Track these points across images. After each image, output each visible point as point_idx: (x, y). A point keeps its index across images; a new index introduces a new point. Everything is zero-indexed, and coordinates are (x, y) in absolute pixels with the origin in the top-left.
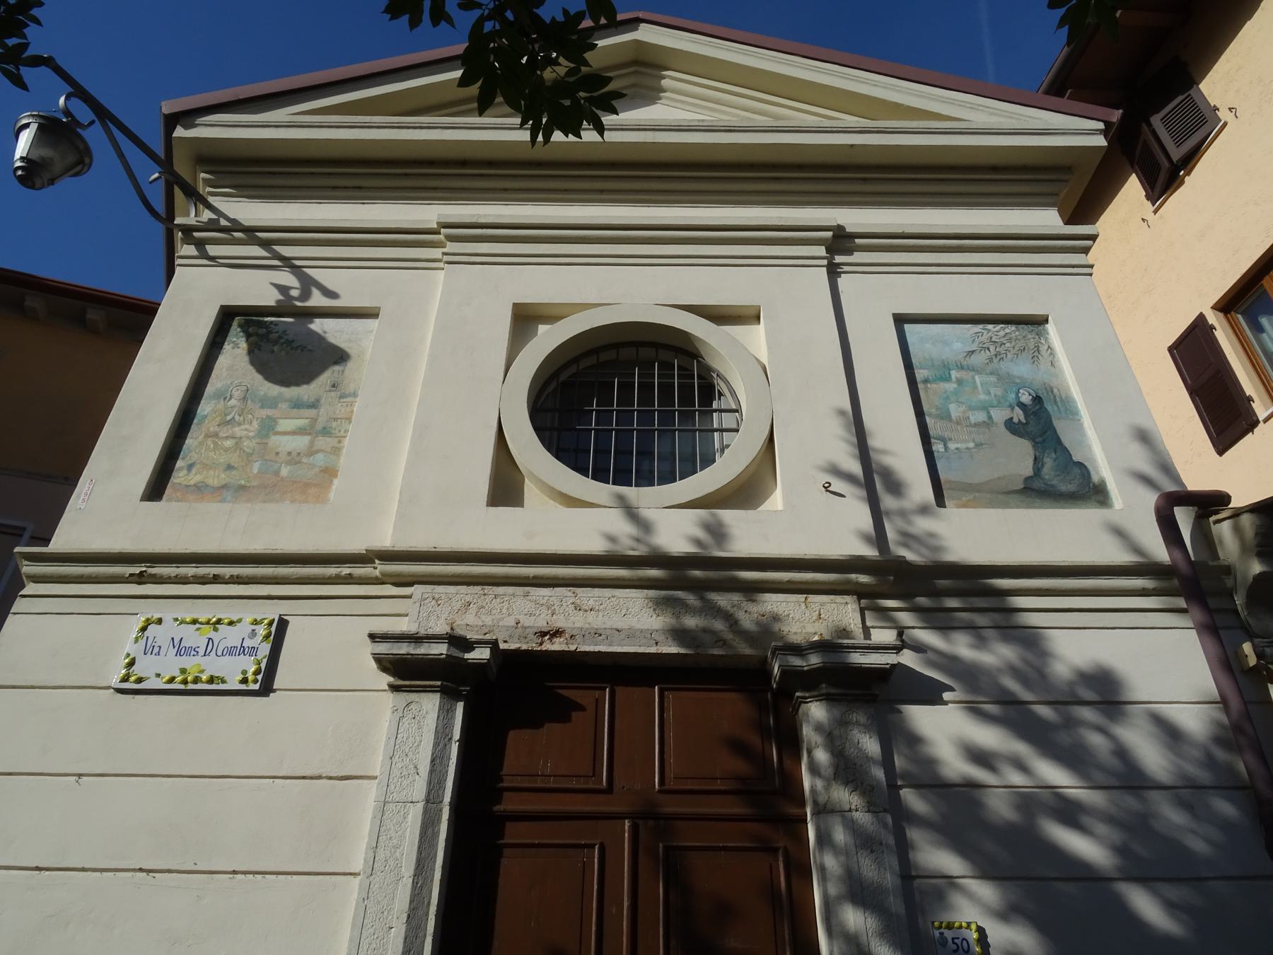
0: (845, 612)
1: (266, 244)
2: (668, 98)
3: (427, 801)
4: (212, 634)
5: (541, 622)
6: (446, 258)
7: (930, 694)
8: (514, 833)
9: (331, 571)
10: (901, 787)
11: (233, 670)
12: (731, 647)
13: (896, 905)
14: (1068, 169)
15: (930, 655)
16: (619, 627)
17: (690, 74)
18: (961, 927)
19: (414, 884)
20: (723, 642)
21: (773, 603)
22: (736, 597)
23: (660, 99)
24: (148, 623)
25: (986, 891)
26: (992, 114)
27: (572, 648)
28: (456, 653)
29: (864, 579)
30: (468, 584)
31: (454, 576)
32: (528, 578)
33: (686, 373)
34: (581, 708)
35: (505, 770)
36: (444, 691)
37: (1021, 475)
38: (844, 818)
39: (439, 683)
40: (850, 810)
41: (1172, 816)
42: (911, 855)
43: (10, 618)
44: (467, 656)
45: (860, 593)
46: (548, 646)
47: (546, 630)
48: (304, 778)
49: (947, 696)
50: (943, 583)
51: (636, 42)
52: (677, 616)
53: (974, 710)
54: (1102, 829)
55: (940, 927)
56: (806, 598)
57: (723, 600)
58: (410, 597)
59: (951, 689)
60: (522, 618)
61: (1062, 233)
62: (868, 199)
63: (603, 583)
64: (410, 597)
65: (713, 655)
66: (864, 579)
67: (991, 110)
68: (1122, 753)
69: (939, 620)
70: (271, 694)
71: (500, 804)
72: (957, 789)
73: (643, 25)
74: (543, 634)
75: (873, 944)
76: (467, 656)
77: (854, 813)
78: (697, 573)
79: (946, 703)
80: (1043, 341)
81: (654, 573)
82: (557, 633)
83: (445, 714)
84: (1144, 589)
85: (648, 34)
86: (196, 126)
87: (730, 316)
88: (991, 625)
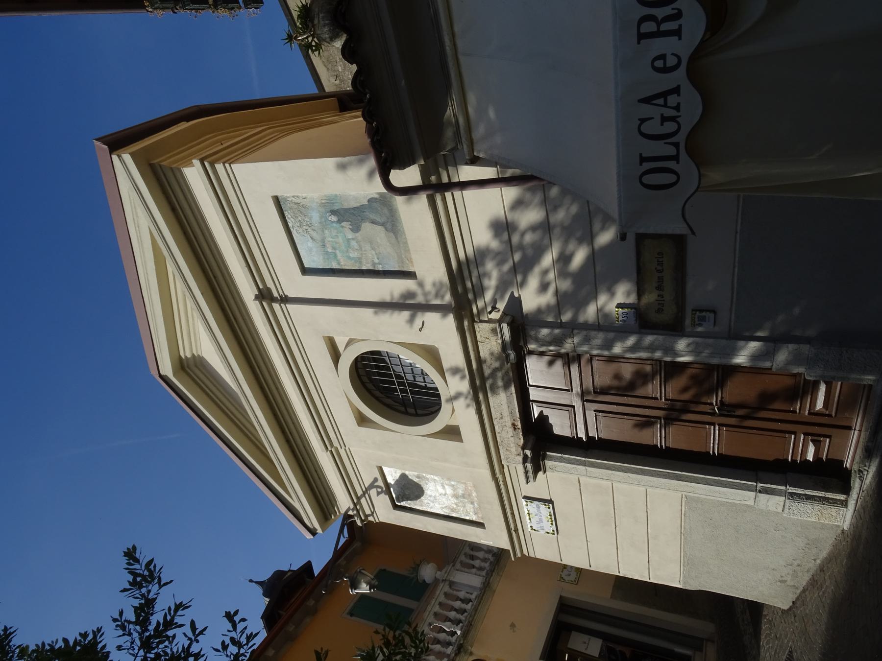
0: (483, 330)
1: (359, 499)
2: (197, 352)
3: (585, 466)
4: (534, 515)
5: (511, 430)
6: (343, 447)
7: (515, 303)
8: (593, 433)
9: (502, 486)
10: (561, 320)
11: (545, 510)
12: (508, 370)
13: (611, 335)
14: (152, 167)
15: (497, 297)
16: (507, 407)
17: (178, 344)
18: (618, 314)
19: (614, 470)
20: (507, 373)
21: (484, 353)
22: (485, 367)
23: (199, 355)
24: (532, 529)
25: (602, 299)
26: (137, 217)
27: (518, 419)
28: (529, 460)
29: (466, 323)
30: (499, 449)
31: (496, 454)
32: (492, 435)
33: (369, 359)
34: (542, 412)
35: (570, 435)
36: (543, 460)
37: (386, 233)
38: (577, 347)
39: (541, 462)
40: (574, 344)
41: (560, 216)
42: (590, 323)
43: (537, 557)
44: (530, 456)
45: (472, 322)
46: (520, 426)
47: (513, 428)
48: (581, 493)
49: (516, 295)
50: (460, 289)
51: (174, 375)
52: (498, 388)
53: (523, 284)
54: (571, 247)
55: (618, 321)
56: (480, 342)
57: (487, 372)
58: (508, 466)
59: (512, 293)
60: (509, 436)
61: (208, 182)
62: (215, 252)
63: (489, 413)
64: (508, 466)
65: (513, 375)
66: (466, 323)
67: (135, 217)
68: (533, 228)
69: (479, 291)
70: (552, 500)
71: (582, 438)
72: (559, 298)
73: (162, 373)
74: (515, 429)
75: (625, 346)
76: (530, 456)
77: (575, 343)
78: (478, 382)
79: (520, 295)
80: (290, 200)
81: (481, 396)
82: (514, 425)
83: (552, 459)
84: (442, 200)
85: (167, 369)
86: (314, 528)
87: (331, 343)
88: (477, 270)
